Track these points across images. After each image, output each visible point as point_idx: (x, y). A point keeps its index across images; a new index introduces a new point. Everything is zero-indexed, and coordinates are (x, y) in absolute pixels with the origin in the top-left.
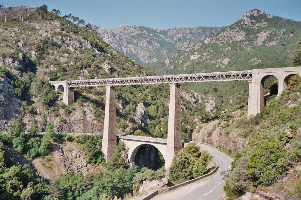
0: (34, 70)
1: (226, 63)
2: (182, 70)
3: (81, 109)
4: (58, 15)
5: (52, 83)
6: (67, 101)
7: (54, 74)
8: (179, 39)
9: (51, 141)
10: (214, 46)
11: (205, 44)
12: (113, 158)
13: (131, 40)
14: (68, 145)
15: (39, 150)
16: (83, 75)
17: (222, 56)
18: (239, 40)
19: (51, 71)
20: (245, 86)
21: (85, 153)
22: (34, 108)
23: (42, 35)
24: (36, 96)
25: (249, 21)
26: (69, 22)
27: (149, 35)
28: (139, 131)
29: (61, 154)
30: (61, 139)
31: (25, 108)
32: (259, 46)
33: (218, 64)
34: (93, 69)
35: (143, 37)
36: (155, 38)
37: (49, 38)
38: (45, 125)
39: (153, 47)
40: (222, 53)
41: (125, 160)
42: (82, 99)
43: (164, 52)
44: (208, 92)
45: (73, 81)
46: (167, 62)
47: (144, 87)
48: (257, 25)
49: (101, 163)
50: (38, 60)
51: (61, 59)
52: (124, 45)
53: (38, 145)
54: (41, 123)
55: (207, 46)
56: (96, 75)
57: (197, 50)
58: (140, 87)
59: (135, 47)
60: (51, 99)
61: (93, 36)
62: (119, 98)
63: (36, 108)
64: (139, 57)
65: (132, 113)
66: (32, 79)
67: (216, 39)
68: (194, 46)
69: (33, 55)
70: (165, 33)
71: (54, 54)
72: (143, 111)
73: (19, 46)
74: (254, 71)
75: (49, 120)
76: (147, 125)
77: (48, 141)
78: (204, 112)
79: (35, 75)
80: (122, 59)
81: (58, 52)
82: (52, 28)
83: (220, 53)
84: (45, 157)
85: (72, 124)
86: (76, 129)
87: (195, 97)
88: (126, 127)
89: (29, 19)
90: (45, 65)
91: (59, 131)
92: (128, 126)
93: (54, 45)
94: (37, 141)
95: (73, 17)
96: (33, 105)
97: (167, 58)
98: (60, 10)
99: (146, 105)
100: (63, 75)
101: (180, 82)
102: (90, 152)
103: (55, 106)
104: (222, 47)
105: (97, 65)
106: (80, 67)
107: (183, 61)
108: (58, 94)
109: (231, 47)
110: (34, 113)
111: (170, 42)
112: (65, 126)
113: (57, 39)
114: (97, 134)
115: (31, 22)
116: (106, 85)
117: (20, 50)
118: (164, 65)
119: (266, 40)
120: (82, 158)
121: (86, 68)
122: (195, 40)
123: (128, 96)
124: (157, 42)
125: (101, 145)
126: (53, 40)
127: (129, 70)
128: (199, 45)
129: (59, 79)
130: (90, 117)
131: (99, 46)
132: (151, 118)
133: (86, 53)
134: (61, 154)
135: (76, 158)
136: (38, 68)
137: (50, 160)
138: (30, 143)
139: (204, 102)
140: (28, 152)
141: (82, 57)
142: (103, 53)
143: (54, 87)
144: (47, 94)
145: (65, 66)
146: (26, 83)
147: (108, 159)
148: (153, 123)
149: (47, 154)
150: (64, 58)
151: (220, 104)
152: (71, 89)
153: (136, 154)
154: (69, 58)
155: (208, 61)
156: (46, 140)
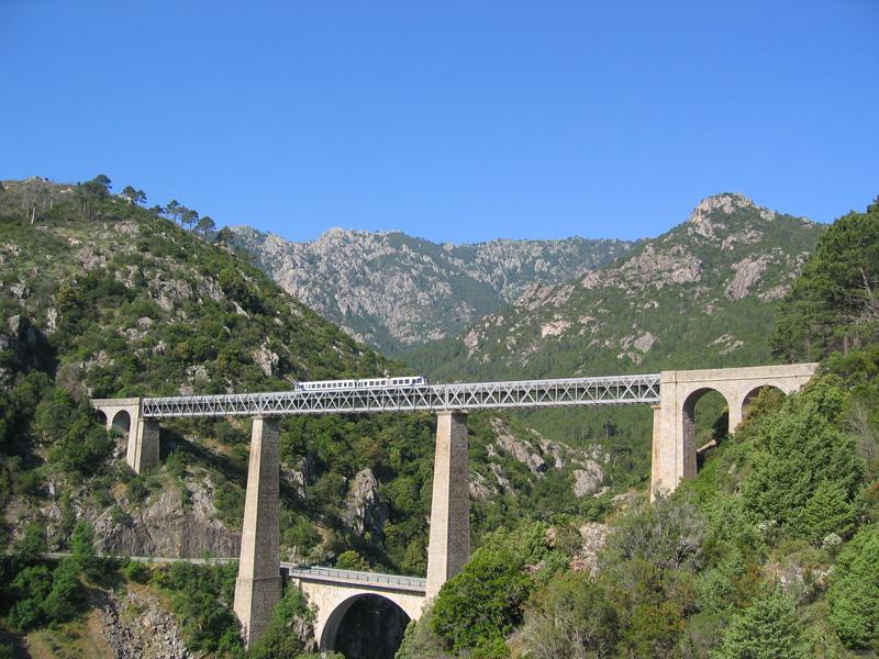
0: (50, 367)
1: (645, 350)
2: (516, 366)
3: (178, 484)
4: (139, 203)
5: (97, 404)
6: (138, 460)
7: (108, 377)
8: (512, 275)
9: (83, 578)
10: (612, 298)
11: (586, 289)
12: (268, 635)
13: (364, 273)
14: (134, 593)
15: (44, 605)
16: (193, 382)
17: (634, 326)
18: (682, 280)
19: (97, 368)
20: (645, 415)
21: (181, 617)
22: (39, 479)
23: (82, 263)
24: (47, 444)
25: (709, 225)
26: (169, 226)
28: (350, 554)
29: (110, 620)
30: (113, 575)
31: (14, 478)
32: (740, 300)
33: (622, 351)
34: (224, 363)
35: (401, 266)
36: (436, 269)
37: (102, 272)
38: (68, 530)
39: (431, 297)
40: (634, 316)
41: (304, 644)
42: (182, 453)
43: (465, 312)
44: (588, 436)
45: (156, 401)
46: (472, 340)
47: (380, 419)
48: (730, 238)
49: (229, 649)
50: (65, 337)
51: (130, 334)
52: (341, 289)
53: (42, 590)
54: (57, 524)
55: (592, 295)
56: (230, 382)
57: (562, 306)
58: (368, 419)
59: (374, 294)
60: (91, 454)
61: (236, 266)
62: (295, 452)
63: (45, 479)
64: (386, 324)
65: (336, 498)
66: (41, 393)
67: (615, 276)
68: (552, 294)
69: (52, 322)
70: (468, 253)
71: (113, 317)
72: (370, 495)
73: (12, 294)
74: (665, 377)
75: (83, 515)
76: (384, 537)
77: (71, 579)
78: (568, 498)
79: (52, 381)
80: (318, 332)
81: (124, 313)
82: (116, 243)
83: (629, 317)
84: (60, 625)
85: (149, 531)
86: (160, 543)
87: (542, 453)
88: (312, 543)
89: (50, 217)
90: (83, 350)
91: (107, 550)
92: (319, 539)
93: (117, 291)
94: (41, 577)
95: (183, 210)
96: (38, 469)
97: (470, 330)
98: (144, 191)
99: (383, 473)
100: (134, 381)
101: (465, 406)
102: (196, 614)
103: (101, 474)
104: (634, 300)
105: (236, 351)
106: (185, 356)
108: (114, 436)
109: (658, 301)
110: (37, 493)
112: (128, 534)
113: (126, 274)
114: (222, 562)
115: (56, 225)
116: (254, 413)
117: (13, 307)
118: (461, 349)
119: (758, 282)
120: (172, 633)
121: (201, 360)
122: (559, 278)
123: (324, 447)
124: (442, 279)
125: (231, 595)
126: (114, 276)
127: (337, 365)
128: (567, 294)
129: (119, 394)
130: (205, 510)
131: (248, 295)
132: (396, 515)
133: (208, 315)
134: (110, 620)
135: (155, 631)
136: (63, 359)
137: (75, 637)
138: (19, 582)
139: (569, 468)
140: (12, 610)
141: (194, 326)
142: (259, 317)
143: (102, 416)
144: (81, 437)
145: (140, 354)
146: (21, 403)
147: (252, 640)
148: (401, 531)
149: (68, 619)
150: (141, 330)
151: (617, 474)
152: (150, 423)
153: (338, 625)
154: (155, 332)
155: (593, 342)
156: (66, 576)
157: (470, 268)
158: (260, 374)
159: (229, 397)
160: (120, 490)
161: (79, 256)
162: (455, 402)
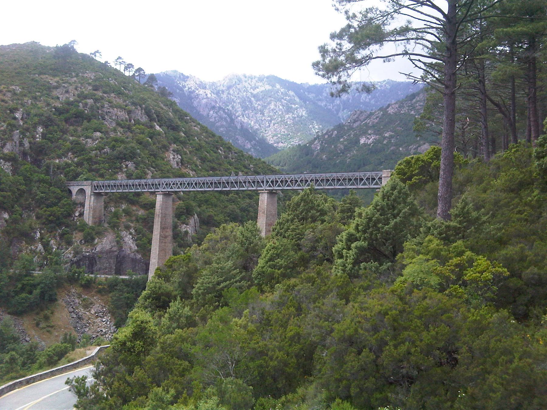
13: (250, 102)
27: (286, 94)
45: (101, 183)
57: (373, 126)
73: (15, 118)
107: (345, 146)
111: (327, 109)
150: (94, 140)
157: (320, 100)
158: (169, 167)
159: (232, 178)
160: (77, 237)
161: (55, 93)
162: (270, 186)
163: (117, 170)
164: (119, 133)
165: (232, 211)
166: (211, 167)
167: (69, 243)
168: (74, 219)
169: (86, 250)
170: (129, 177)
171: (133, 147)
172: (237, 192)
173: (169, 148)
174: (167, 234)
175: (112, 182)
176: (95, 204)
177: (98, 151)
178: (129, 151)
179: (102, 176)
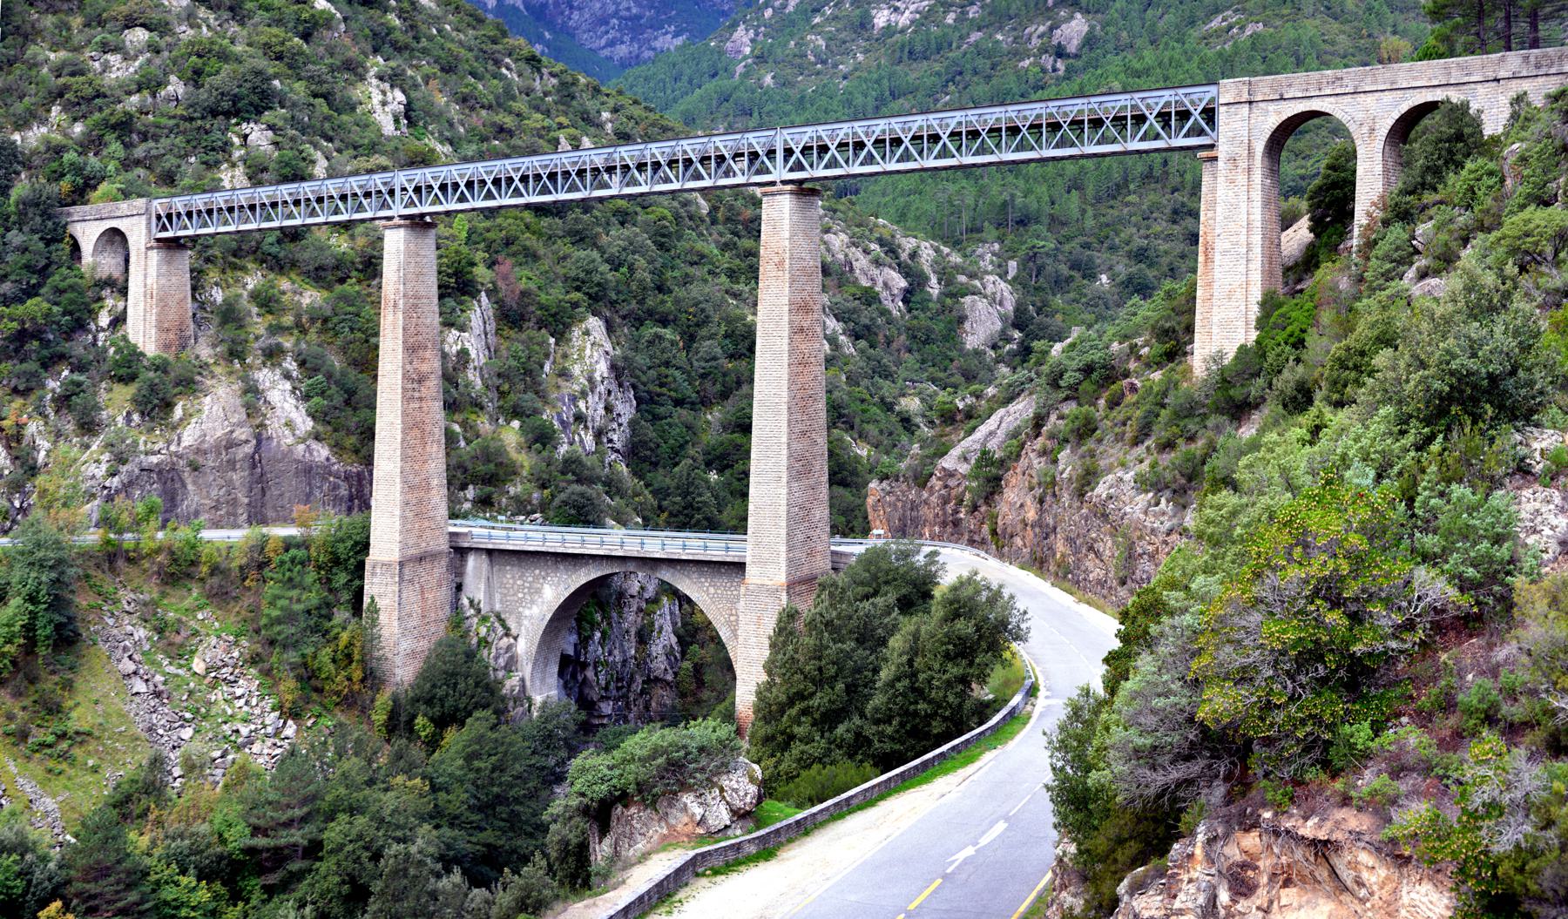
45: (179, 204)
74: (1228, 90)
107: (830, 39)
139: (954, 293)
160: (115, 403)
163: (211, 157)
164: (204, 29)
165: (588, 272)
166: (494, 124)
167: (88, 427)
168: (95, 339)
169: (153, 448)
170: (257, 173)
171: (258, 73)
172: (585, 205)
173: (366, 70)
174: (425, 368)
175: (199, 201)
176: (163, 281)
177: (146, 93)
178: (248, 85)
179: (169, 179)
